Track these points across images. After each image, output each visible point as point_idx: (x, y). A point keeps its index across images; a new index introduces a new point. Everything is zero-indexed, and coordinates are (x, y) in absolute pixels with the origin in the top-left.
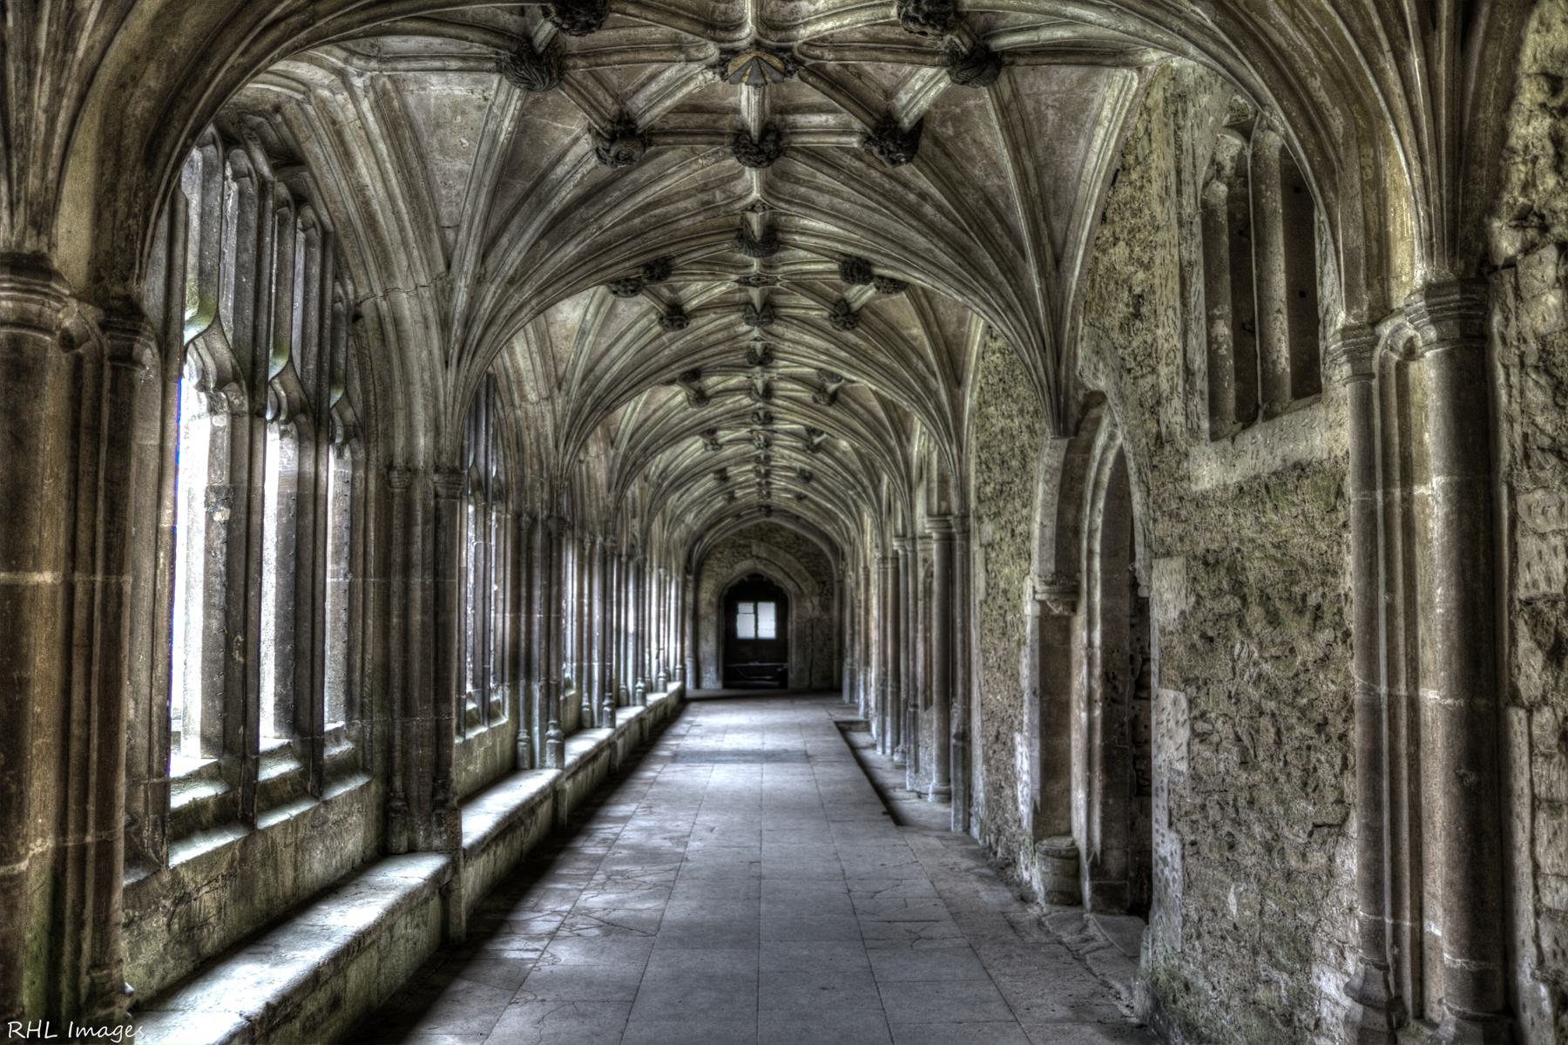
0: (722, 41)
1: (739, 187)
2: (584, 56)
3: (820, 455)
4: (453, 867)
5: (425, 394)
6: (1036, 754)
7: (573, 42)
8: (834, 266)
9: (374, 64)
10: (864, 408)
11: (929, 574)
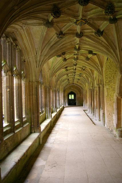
0: (76, 19)
1: (75, 41)
2: (56, 22)
4: (40, 134)
5: (34, 72)
6: (117, 117)
7: (55, 20)
8: (87, 52)
9: (26, 25)
11: (97, 92)
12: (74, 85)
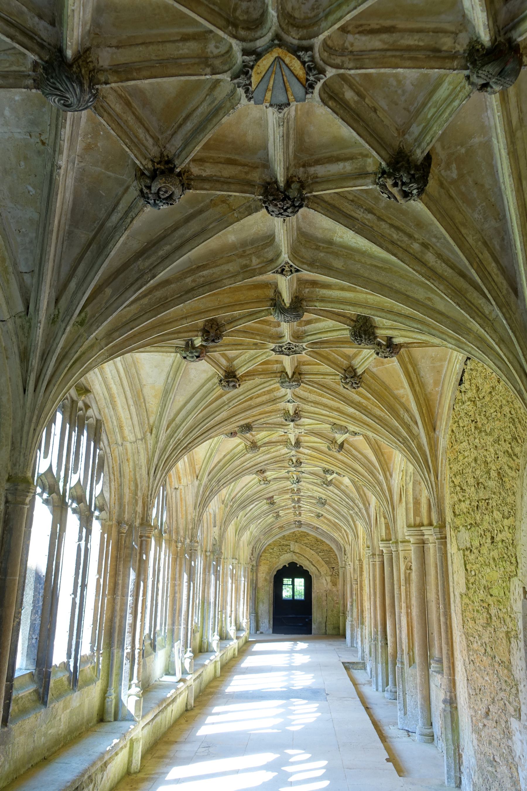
3: (331, 488)
10: (361, 454)
12: (302, 529)
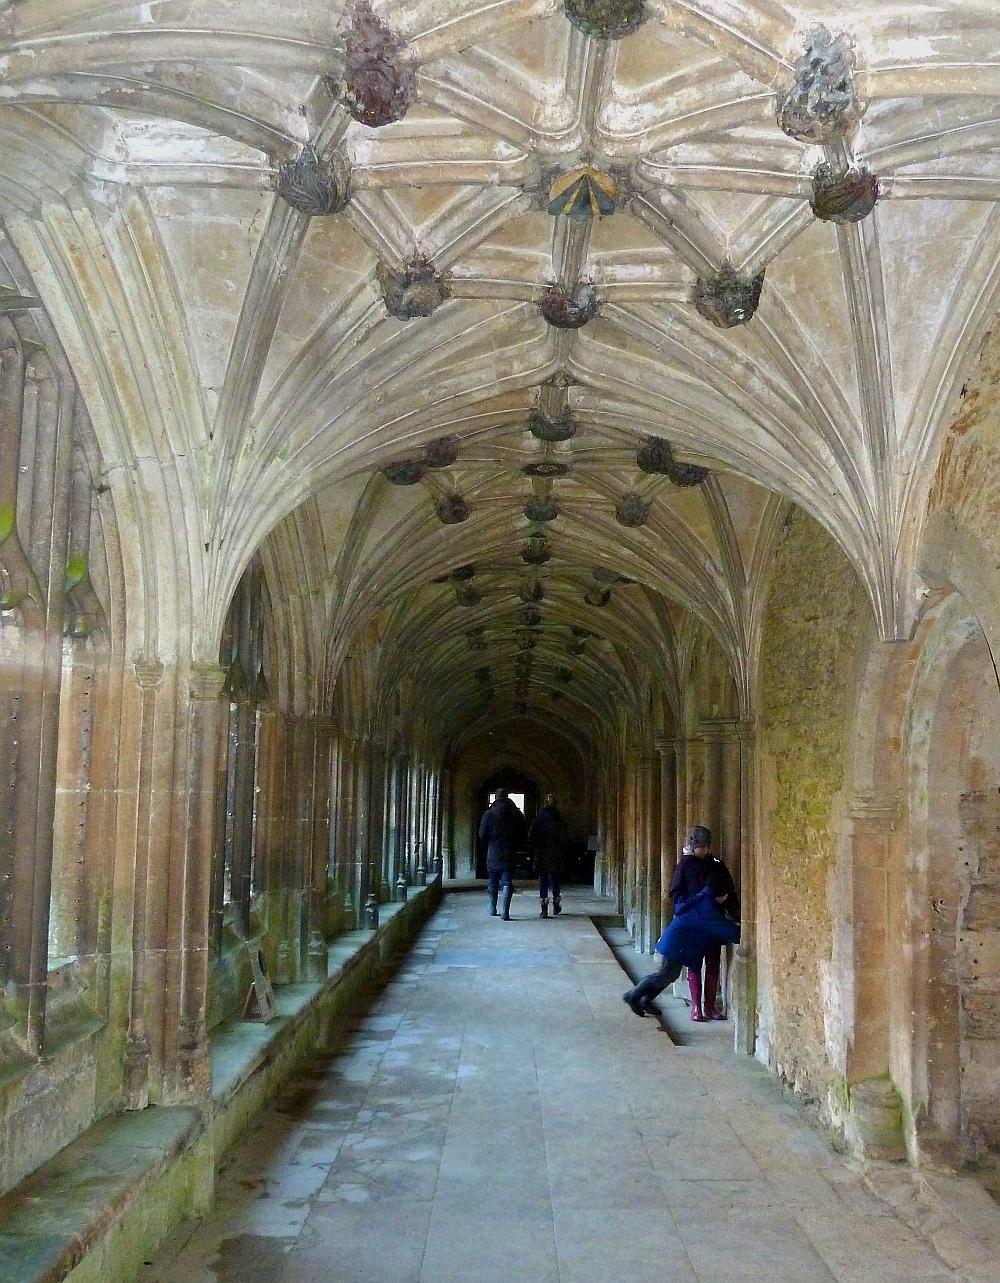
6: (850, 986)
12: (527, 716)
